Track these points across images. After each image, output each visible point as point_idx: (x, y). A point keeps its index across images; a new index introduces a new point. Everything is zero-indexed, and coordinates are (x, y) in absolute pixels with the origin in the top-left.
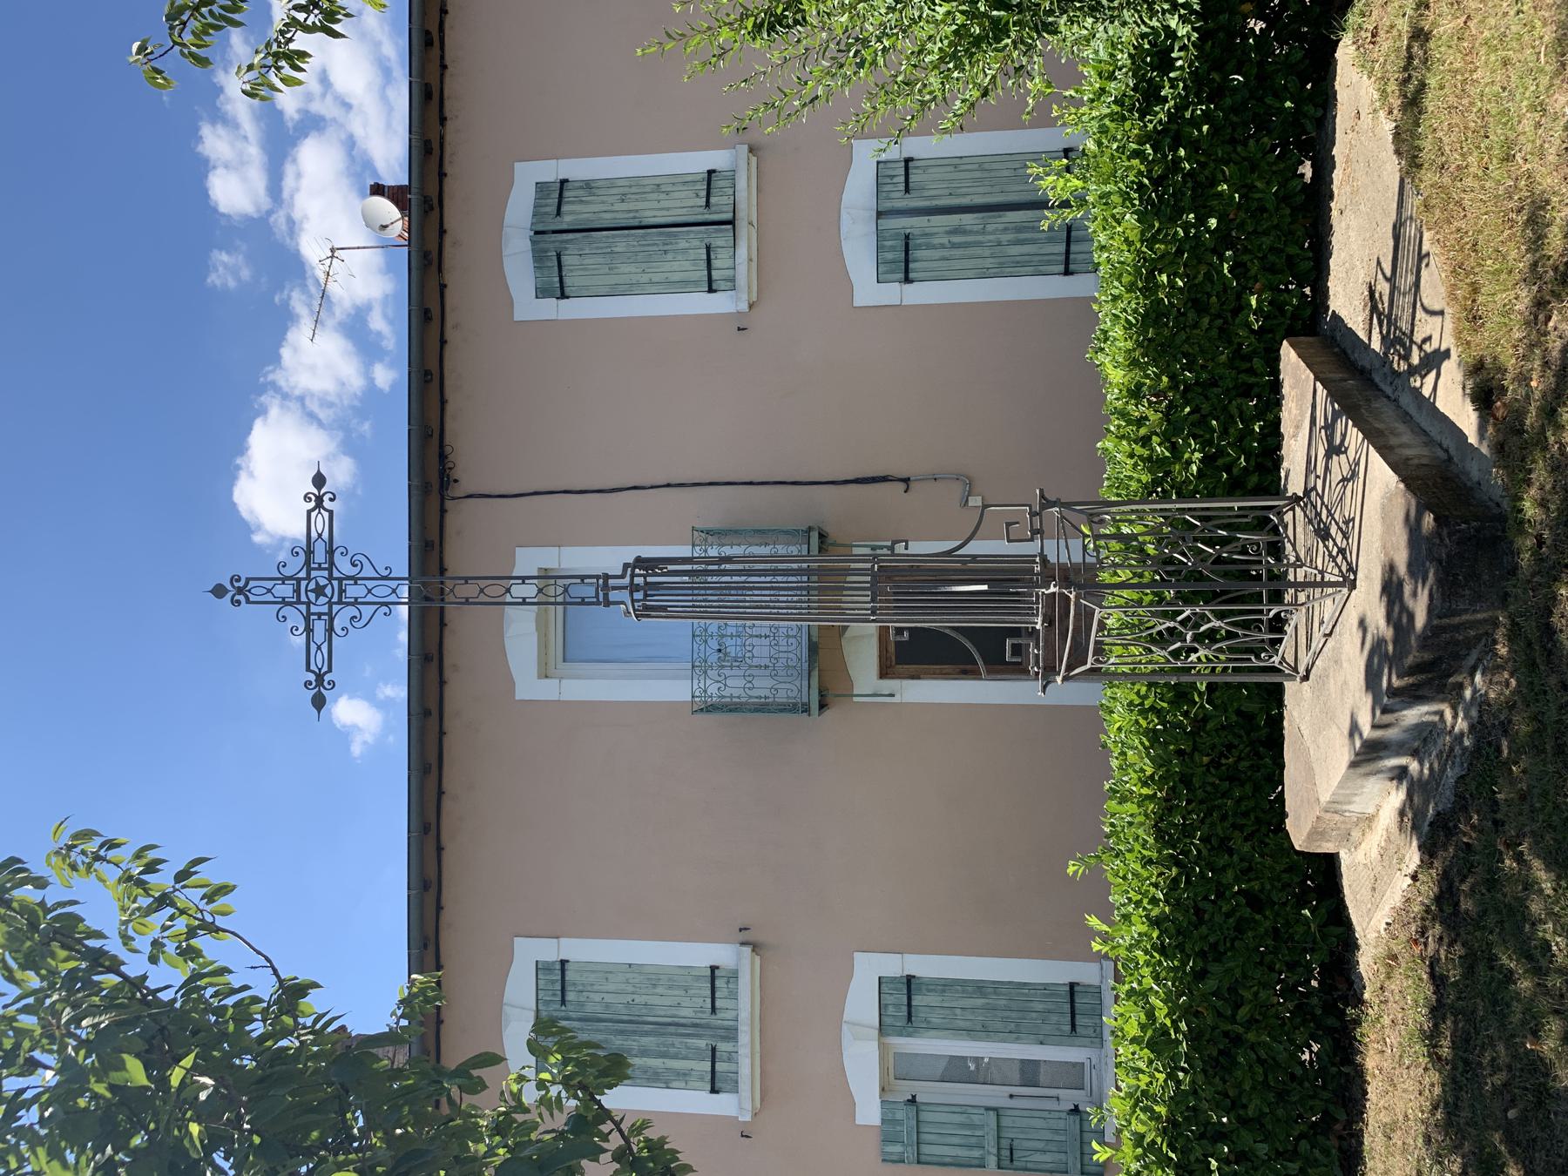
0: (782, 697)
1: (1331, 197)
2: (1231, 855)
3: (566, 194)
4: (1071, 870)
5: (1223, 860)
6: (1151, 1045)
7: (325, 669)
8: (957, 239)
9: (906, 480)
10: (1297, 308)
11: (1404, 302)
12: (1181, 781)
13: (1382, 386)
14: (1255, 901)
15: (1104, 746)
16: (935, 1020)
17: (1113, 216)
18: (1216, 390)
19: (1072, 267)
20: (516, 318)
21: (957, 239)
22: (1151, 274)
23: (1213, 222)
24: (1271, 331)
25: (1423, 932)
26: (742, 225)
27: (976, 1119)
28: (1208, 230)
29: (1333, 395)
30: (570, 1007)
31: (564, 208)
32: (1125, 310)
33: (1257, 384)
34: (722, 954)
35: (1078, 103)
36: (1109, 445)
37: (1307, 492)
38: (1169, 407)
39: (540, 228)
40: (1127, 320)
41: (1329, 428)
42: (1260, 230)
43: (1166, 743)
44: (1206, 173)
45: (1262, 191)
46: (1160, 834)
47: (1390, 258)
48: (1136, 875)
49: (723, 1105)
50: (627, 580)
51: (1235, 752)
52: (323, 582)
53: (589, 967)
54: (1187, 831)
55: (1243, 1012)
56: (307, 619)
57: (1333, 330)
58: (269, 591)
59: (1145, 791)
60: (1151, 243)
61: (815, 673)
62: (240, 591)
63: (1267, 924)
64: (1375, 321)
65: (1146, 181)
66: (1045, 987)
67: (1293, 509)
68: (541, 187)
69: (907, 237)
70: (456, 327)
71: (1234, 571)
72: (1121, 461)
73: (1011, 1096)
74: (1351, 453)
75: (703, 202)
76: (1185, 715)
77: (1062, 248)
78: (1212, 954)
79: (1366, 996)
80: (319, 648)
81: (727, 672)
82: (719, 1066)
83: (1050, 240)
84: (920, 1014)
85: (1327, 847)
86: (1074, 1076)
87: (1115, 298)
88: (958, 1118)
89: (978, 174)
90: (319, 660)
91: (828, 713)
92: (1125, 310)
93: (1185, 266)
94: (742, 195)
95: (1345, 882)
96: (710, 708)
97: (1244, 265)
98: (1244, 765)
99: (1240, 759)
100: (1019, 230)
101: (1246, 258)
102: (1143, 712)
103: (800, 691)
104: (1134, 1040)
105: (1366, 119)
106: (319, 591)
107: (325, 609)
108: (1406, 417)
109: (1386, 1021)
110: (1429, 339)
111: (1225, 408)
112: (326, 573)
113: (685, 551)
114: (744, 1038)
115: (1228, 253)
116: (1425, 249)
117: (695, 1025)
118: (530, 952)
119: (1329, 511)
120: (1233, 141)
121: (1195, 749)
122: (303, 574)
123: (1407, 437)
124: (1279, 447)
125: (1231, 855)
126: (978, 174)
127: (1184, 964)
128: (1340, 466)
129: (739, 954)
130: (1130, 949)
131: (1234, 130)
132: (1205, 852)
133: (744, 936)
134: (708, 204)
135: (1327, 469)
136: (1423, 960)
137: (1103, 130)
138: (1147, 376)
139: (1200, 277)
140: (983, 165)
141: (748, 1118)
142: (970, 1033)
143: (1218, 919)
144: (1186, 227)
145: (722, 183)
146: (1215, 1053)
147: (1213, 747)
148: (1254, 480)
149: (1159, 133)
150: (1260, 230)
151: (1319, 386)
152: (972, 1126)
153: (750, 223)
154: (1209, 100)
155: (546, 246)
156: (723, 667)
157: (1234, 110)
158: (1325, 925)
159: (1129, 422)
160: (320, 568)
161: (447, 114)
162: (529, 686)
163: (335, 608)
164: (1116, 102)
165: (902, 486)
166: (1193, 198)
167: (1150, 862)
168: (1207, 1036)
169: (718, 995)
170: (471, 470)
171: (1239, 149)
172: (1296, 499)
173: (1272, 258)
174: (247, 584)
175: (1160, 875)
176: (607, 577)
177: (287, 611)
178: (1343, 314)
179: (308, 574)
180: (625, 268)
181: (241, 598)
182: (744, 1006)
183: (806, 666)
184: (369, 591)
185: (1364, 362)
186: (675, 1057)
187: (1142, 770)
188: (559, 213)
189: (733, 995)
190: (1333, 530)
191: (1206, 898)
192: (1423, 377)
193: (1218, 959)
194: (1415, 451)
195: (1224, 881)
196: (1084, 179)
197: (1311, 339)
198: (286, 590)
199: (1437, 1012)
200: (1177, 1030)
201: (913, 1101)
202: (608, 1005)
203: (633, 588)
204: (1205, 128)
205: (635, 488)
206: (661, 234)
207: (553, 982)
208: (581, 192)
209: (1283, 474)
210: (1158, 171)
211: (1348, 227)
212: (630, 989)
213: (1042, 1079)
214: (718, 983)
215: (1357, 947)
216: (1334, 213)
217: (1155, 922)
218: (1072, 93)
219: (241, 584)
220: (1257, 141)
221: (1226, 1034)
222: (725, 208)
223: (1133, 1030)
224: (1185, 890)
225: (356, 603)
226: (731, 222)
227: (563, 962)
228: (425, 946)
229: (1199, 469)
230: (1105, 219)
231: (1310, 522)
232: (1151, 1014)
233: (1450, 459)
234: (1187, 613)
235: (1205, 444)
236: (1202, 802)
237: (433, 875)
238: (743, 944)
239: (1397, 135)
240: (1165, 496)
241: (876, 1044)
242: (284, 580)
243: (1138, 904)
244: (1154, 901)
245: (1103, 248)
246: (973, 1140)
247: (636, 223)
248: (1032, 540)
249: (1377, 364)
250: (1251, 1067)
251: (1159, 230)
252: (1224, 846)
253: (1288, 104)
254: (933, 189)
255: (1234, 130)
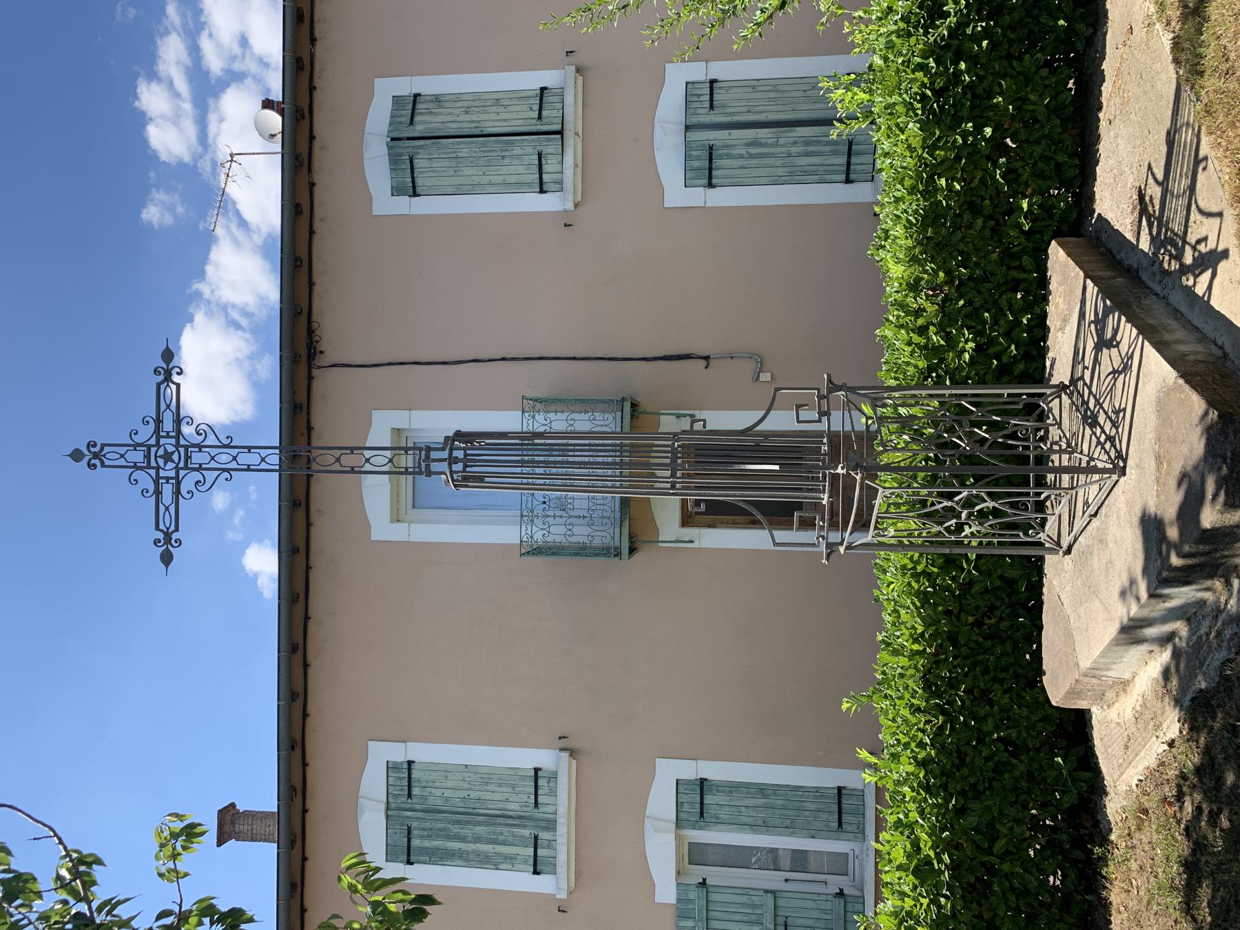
0: (597, 542)
1: (1100, 109)
2: (992, 706)
3: (419, 106)
4: (845, 706)
5: (982, 711)
6: (916, 873)
7: (172, 528)
8: (753, 151)
9: (707, 358)
10: (1065, 211)
11: (1176, 206)
12: (949, 638)
13: (1150, 283)
14: (1013, 747)
15: (877, 600)
16: (724, 817)
17: (897, 125)
18: (989, 286)
19: (852, 176)
20: (375, 213)
21: (753, 151)
22: (931, 178)
23: (988, 131)
24: (1039, 232)
25: (1180, 797)
26: (569, 134)
27: (756, 900)
28: (984, 138)
29: (1104, 291)
30: (415, 800)
31: (417, 119)
32: (905, 211)
33: (1025, 280)
34: (545, 758)
35: (867, 22)
36: (889, 333)
37: (1073, 381)
38: (944, 301)
39: (396, 135)
40: (908, 220)
41: (1100, 323)
42: (1032, 139)
43: (936, 604)
44: (985, 85)
45: (1035, 104)
46: (927, 685)
47: (1163, 163)
48: (906, 721)
49: (544, 884)
50: (445, 454)
51: (997, 613)
52: (170, 449)
53: (431, 767)
54: (953, 684)
55: (1000, 845)
56: (156, 482)
57: (1098, 232)
58: (122, 456)
59: (916, 647)
60: (932, 149)
61: (626, 523)
62: (96, 455)
63: (1023, 768)
64: (1144, 222)
65: (929, 92)
66: (817, 790)
67: (1060, 397)
68: (397, 100)
69: (711, 148)
70: (322, 220)
71: (998, 446)
72: (899, 348)
73: (786, 880)
74: (1124, 347)
75: (536, 114)
76: (954, 579)
77: (843, 160)
78: (972, 793)
79: (1113, 837)
80: (167, 509)
81: (550, 520)
82: (540, 852)
83: (834, 153)
84: (710, 811)
85: (1081, 704)
86: (840, 864)
87: (897, 200)
88: (744, 899)
89: (773, 95)
90: (167, 521)
91: (637, 556)
92: (905, 211)
93: (963, 170)
94: (569, 110)
95: (1096, 734)
96: (537, 551)
97: (1015, 171)
98: (1005, 625)
99: (1001, 619)
100: (808, 144)
101: (1018, 164)
102: (916, 576)
103: (613, 538)
104: (899, 868)
105: (1140, 33)
106: (168, 457)
107: (172, 474)
108: (1177, 314)
109: (1134, 866)
110: (1205, 239)
111: (995, 302)
112: (173, 441)
113: (509, 421)
114: (562, 829)
115: (1002, 160)
116: (1202, 154)
117: (520, 817)
118: (381, 754)
119: (1097, 401)
120: (1009, 56)
121: (961, 610)
122: (153, 441)
123: (1180, 334)
124: (1045, 339)
125: (992, 706)
126: (773, 95)
127: (947, 801)
128: (1111, 360)
129: (558, 758)
130: (898, 783)
131: (1010, 46)
132: (968, 703)
133: (563, 743)
134: (540, 117)
135: (1096, 361)
136: (1179, 822)
137: (890, 46)
138: (925, 272)
139: (976, 182)
140: (776, 86)
141: (564, 896)
142: (753, 827)
143: (979, 762)
144: (965, 134)
145: (551, 99)
146: (972, 880)
147: (977, 608)
148: (1021, 366)
149: (942, 48)
150: (1032, 139)
151: (1090, 283)
152: (754, 906)
153: (577, 134)
154: (989, 18)
155: (400, 151)
156: (547, 516)
157: (1012, 28)
158: (1075, 770)
159: (908, 313)
160: (168, 436)
161: (317, 35)
162: (383, 529)
163: (182, 473)
164: (902, 19)
165: (703, 363)
166: (972, 108)
167: (918, 710)
168: (966, 866)
169: (540, 792)
170: (334, 345)
171: (1015, 63)
172: (1062, 387)
173: (1041, 165)
174: (102, 449)
175: (928, 722)
176: (429, 449)
177: (138, 475)
178: (1109, 216)
179: (158, 441)
180: (468, 171)
181: (97, 462)
182: (562, 803)
183: (618, 515)
184: (213, 458)
185: (1131, 261)
186: (504, 843)
187: (913, 627)
188: (412, 123)
189: (553, 793)
190: (1102, 418)
191: (968, 743)
192: (1196, 276)
193: (978, 796)
194: (1189, 347)
195: (985, 729)
196: (871, 92)
197: (1074, 239)
198: (137, 456)
199: (1191, 867)
200: (940, 861)
201: (703, 883)
202: (447, 799)
203: (452, 461)
204: (985, 43)
205: (475, 361)
206: (497, 142)
207: (401, 779)
208: (431, 105)
209: (1048, 363)
210: (939, 83)
211: (1117, 136)
212: (466, 786)
213: (812, 867)
214: (540, 782)
215: (1106, 794)
216: (1103, 124)
217: (922, 764)
218: (861, 13)
219: (97, 449)
220: (1032, 56)
221: (983, 864)
222: (555, 121)
223: (899, 856)
224: (949, 736)
225: (200, 468)
226: (560, 133)
227: (410, 763)
228: (293, 748)
229: (971, 357)
230: (889, 128)
231: (1077, 410)
232: (916, 847)
233: (1225, 355)
234: (965, 494)
235: (978, 334)
236: (966, 658)
237: (300, 689)
238: (562, 750)
239: (1176, 45)
240: (939, 383)
241: (671, 837)
242: (136, 446)
243: (906, 746)
244: (921, 745)
245: (886, 155)
246: (753, 918)
247: (477, 132)
248: (819, 421)
249: (1145, 263)
250: (1004, 893)
251: (939, 138)
252: (984, 697)
253: (1062, 22)
254: (734, 106)
255: (1010, 46)
